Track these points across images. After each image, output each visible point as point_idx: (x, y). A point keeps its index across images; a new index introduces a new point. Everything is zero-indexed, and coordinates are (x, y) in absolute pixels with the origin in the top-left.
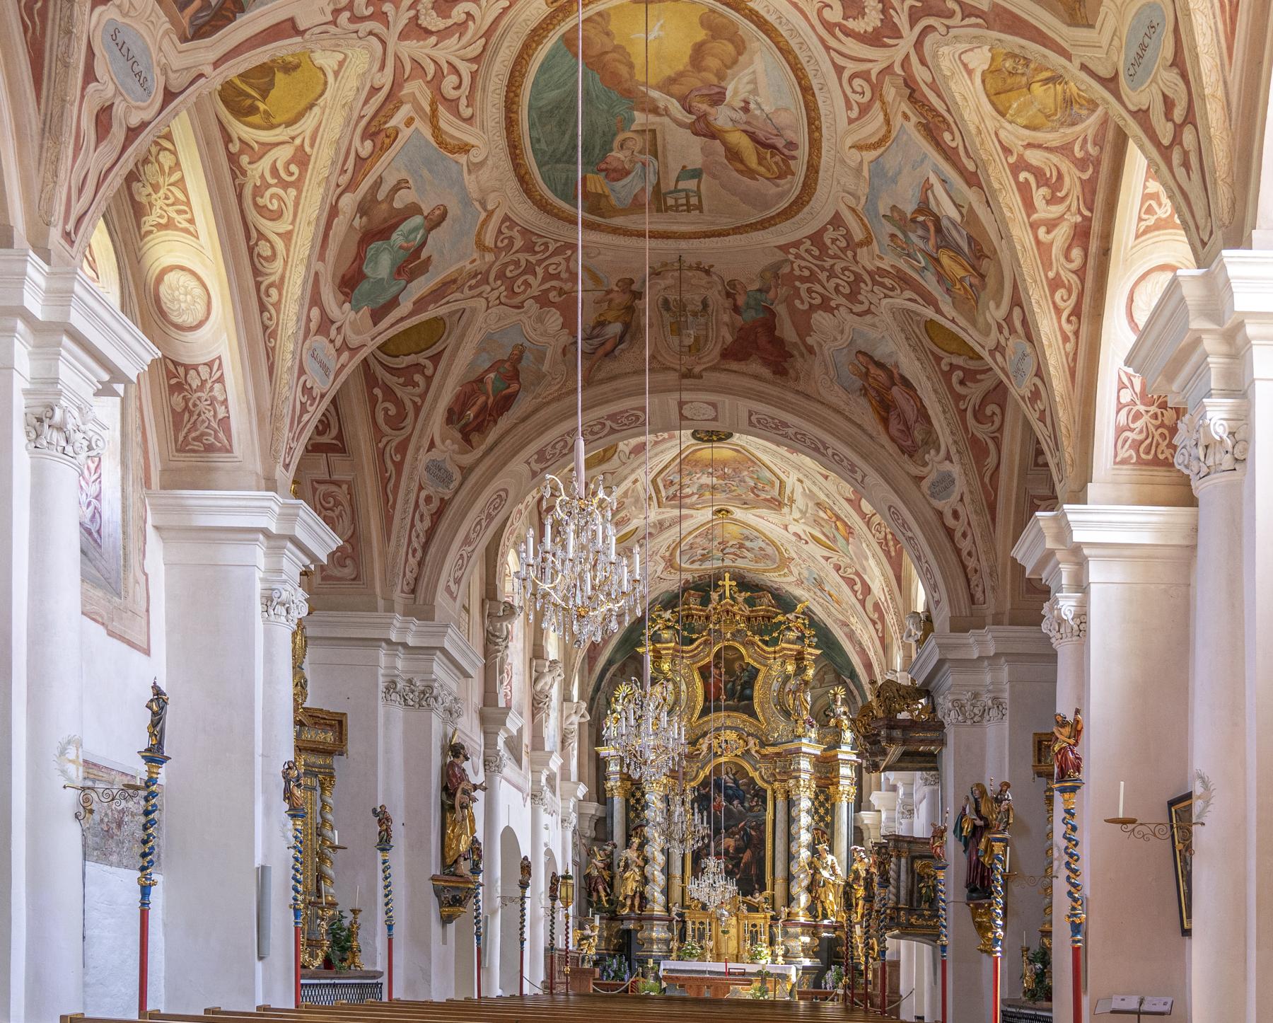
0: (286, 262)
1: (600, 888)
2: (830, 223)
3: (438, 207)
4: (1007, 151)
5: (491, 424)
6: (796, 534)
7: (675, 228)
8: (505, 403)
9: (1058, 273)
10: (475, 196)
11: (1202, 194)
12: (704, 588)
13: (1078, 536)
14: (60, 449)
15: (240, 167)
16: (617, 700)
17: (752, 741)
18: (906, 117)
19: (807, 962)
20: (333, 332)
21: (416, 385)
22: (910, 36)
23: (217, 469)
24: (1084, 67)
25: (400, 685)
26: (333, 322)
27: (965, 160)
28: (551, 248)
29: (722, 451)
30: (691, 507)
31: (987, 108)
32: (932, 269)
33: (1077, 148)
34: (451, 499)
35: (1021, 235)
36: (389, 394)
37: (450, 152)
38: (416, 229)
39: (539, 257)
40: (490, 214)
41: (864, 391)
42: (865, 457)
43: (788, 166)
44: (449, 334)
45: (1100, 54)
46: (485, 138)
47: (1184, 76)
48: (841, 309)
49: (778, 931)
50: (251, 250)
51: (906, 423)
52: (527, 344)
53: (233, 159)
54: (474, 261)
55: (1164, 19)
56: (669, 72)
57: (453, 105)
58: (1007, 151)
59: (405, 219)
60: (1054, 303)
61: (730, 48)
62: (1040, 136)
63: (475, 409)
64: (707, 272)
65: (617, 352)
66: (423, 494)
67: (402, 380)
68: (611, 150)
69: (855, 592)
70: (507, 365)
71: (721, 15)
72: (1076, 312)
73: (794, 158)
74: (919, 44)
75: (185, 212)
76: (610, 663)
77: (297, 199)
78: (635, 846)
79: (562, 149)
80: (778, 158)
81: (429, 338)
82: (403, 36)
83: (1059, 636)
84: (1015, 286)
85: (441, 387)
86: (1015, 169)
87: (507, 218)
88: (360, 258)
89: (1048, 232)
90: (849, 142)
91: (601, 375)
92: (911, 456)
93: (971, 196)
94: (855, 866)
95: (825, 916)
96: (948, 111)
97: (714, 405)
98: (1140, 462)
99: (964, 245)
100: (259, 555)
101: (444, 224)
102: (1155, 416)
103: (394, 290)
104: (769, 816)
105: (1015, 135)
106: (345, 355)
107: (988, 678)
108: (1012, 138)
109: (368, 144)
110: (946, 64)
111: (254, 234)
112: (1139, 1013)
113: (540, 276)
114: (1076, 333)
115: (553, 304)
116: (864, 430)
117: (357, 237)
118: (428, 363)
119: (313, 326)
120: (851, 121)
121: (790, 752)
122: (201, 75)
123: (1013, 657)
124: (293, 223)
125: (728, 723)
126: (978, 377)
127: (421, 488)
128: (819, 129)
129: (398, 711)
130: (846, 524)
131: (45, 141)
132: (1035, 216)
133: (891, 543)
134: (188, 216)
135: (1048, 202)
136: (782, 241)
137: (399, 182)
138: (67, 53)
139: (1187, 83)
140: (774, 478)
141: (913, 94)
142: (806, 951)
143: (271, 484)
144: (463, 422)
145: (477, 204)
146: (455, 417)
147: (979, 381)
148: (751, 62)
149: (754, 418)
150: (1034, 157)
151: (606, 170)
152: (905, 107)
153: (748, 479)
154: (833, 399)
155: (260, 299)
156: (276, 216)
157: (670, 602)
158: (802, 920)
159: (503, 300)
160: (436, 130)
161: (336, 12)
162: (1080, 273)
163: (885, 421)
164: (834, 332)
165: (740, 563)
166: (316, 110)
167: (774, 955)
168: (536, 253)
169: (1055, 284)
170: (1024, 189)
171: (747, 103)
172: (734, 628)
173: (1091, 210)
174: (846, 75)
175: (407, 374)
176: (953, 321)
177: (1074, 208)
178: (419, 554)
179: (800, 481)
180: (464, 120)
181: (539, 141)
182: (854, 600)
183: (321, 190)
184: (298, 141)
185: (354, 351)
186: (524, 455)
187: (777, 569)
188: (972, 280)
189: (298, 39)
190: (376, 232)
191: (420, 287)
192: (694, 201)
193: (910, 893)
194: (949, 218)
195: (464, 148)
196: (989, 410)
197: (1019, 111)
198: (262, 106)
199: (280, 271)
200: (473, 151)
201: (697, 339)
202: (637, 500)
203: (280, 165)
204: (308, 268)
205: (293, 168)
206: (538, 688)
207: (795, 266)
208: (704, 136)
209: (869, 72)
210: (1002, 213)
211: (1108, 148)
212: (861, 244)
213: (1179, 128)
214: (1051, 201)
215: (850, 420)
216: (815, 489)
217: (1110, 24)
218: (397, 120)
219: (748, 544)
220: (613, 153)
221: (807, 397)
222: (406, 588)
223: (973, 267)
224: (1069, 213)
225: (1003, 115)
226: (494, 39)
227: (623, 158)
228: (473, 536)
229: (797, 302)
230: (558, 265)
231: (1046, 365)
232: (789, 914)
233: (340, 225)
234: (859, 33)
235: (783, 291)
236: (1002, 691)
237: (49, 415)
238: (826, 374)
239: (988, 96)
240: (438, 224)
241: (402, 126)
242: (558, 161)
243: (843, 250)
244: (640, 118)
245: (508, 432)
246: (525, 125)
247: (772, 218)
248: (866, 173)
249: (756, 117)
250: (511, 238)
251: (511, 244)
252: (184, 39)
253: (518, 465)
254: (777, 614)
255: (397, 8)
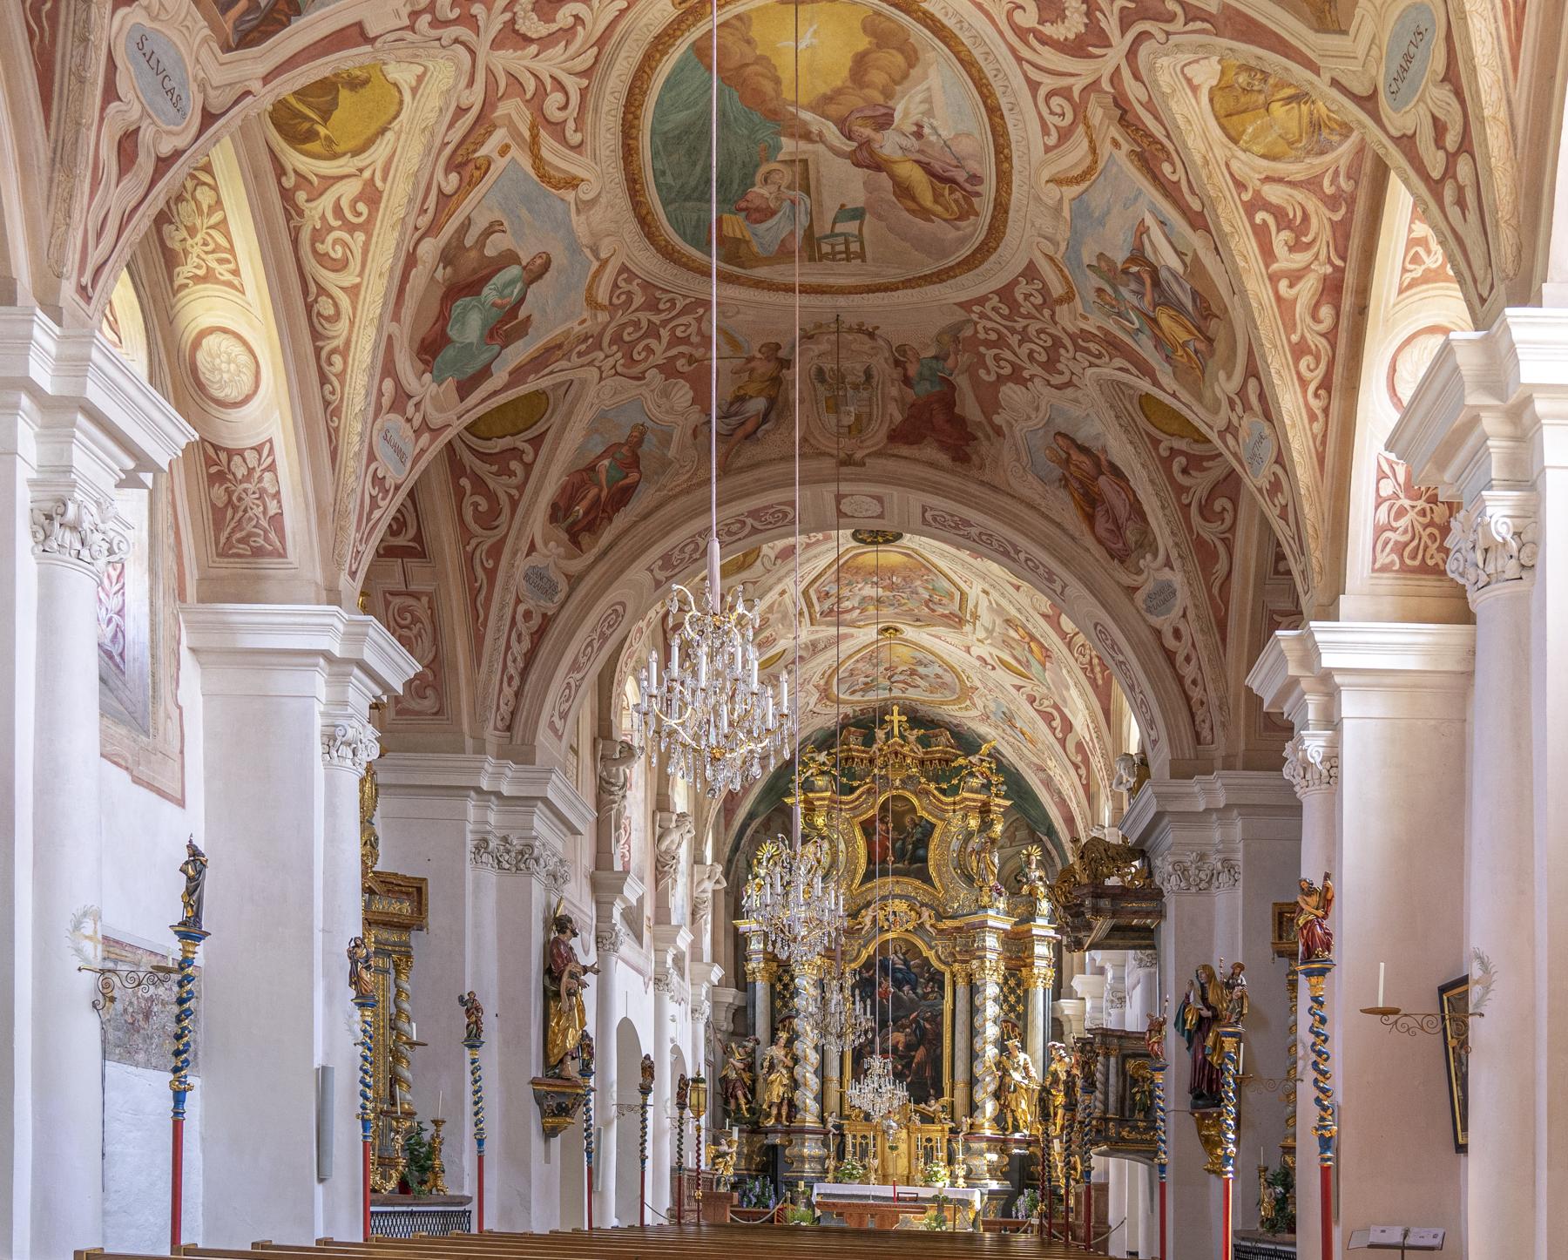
0: (352, 323)
1: (740, 1093)
2: (1022, 275)
3: (539, 255)
4: (1240, 186)
5: (605, 522)
6: (980, 658)
7: (831, 281)
8: (622, 496)
9: (1303, 337)
10: (585, 241)
11: (1481, 239)
12: (867, 724)
13: (1328, 660)
14: (74, 553)
15: (295, 206)
16: (760, 863)
17: (926, 913)
18: (1116, 144)
19: (994, 1185)
20: (410, 409)
21: (512, 474)
22: (1121, 44)
23: (267, 578)
24: (1335, 83)
25: (493, 844)
26: (410, 397)
27: (1188, 197)
28: (679, 306)
29: (890, 556)
30: (852, 624)
31: (1216, 132)
32: (1148, 332)
33: (1326, 182)
34: (556, 615)
35: (1258, 289)
36: (480, 485)
37: (555, 187)
38: (512, 282)
39: (663, 316)
40: (604, 264)
41: (1064, 482)
42: (1065, 563)
43: (971, 205)
44: (553, 411)
45: (1355, 66)
46: (597, 171)
47: (1458, 94)
48: (1036, 380)
49: (959, 1146)
50: (309, 308)
51: (1115, 521)
52: (649, 423)
53: (287, 195)
54: (584, 321)
55: (1434, 24)
56: (823, 89)
57: (557, 129)
58: (1240, 186)
59: (499, 270)
60: (1298, 373)
61: (899, 59)
62: (1280, 168)
63: (585, 503)
64: (871, 335)
65: (759, 434)
66: (521, 609)
67: (495, 468)
68: (753, 185)
69: (1053, 730)
70: (624, 450)
71: (888, 19)
72: (1326, 384)
73: (978, 194)
74: (1131, 54)
75: (228, 261)
76: (751, 816)
77: (366, 245)
78: (782, 1042)
79: (693, 183)
80: (958, 195)
81: (528, 416)
82: (496, 44)
83: (1304, 783)
84: (1250, 353)
85: (543, 476)
86: (1250, 209)
87: (624, 269)
88: (443, 317)
89: (1291, 286)
90: (1046, 175)
91: (741, 462)
92: (1122, 562)
93: (1196, 241)
94: (1054, 1066)
95: (1016, 1129)
96: (1168, 136)
97: (879, 499)
98: (1405, 569)
99: (1188, 302)
100: (319, 683)
101: (547, 276)
102: (1423, 513)
103: (486, 357)
104: (947, 1005)
105: (1250, 166)
106: (426, 437)
107: (1217, 835)
108: (1247, 170)
109: (454, 177)
110: (1165, 79)
111: (313, 289)
112: (1403, 1248)
113: (665, 340)
114: (1326, 411)
115: (681, 375)
116: (1064, 530)
117: (440, 292)
118: (527, 447)
119: (386, 401)
120: (1048, 149)
121: (973, 926)
122: (248, 93)
123: (1248, 810)
124: (361, 275)
125: (897, 890)
126: (1205, 464)
127: (518, 601)
128: (1009, 159)
129: (491, 876)
130: (1042, 646)
131: (56, 174)
132: (1275, 267)
133: (1098, 669)
134: (232, 266)
135: (1291, 249)
136: (964, 297)
137: (492, 224)
138: (83, 65)
139: (1462, 102)
140: (953, 589)
141: (1124, 116)
142: (993, 1171)
143: (333, 596)
144: (570, 520)
145: (587, 252)
146: (560, 514)
147: (1205, 469)
148: (925, 76)
149: (928, 515)
150: (1274, 193)
151: (747, 209)
152: (1115, 132)
153: (921, 590)
154: (1026, 492)
155: (320, 368)
156: (341, 266)
157: (825, 741)
158: (988, 1133)
159: (619, 369)
160: (537, 160)
161: (414, 15)
162: (1331, 336)
163: (1090, 519)
164: (1027, 409)
165: (912, 694)
166: (389, 135)
167: (953, 1177)
168: (660, 311)
169: (1300, 350)
170: (1261, 233)
171: (920, 127)
172: (904, 774)
173: (1344, 259)
174: (1042, 92)
175: (501, 460)
176: (1174, 395)
177: (1323, 256)
178: (516, 682)
179: (986, 592)
180: (572, 148)
181: (663, 173)
182: (1052, 739)
183: (396, 234)
184: (367, 174)
185: (436, 432)
186: (645, 560)
187: (958, 700)
188: (1198, 345)
189: (367, 48)
190: (463, 286)
191: (518, 353)
192: (855, 247)
193: (1121, 1100)
194: (1169, 269)
195: (572, 183)
196: (1218, 505)
197: (1255, 137)
198: (322, 131)
199: (345, 334)
200: (583, 186)
201: (858, 417)
202: (785, 616)
203: (345, 204)
204: (380, 329)
205: (361, 207)
206: (663, 847)
207: (980, 327)
208: (868, 167)
209: (1070, 88)
210: (1234, 262)
211: (1365, 182)
212: (1060, 301)
213: (1452, 158)
214: (1294, 248)
215: (1047, 517)
216: (1004, 603)
217: (1368, 29)
218: (489, 148)
219: (921, 670)
220: (755, 189)
221: (995, 488)
222: (500, 724)
223: (1199, 329)
224: (1317, 263)
225: (1236, 142)
226: (608, 48)
227: (767, 195)
228: (582, 660)
229: (982, 372)
230: (688, 326)
231: (1289, 449)
232: (972, 1126)
233: (419, 277)
234: (1058, 41)
235: (965, 359)
236: (1234, 851)
237: (60, 511)
238: (1018, 460)
239: (1217, 118)
240: (540, 276)
241: (495, 155)
242: (688, 198)
243: (1039, 308)
244: (788, 145)
245: (625, 532)
246: (646, 154)
247: (951, 268)
248: (1066, 213)
249: (931, 144)
250: (629, 294)
251: (630, 300)
252: (227, 49)
253: (638, 573)
254: (957, 756)
255: (489, 10)
